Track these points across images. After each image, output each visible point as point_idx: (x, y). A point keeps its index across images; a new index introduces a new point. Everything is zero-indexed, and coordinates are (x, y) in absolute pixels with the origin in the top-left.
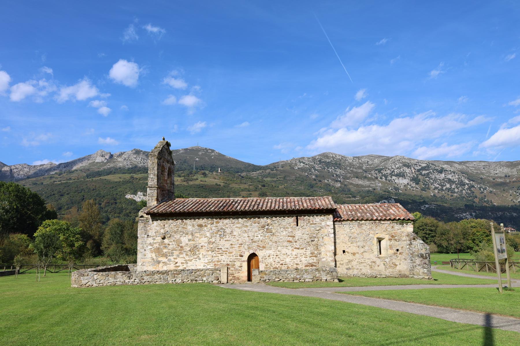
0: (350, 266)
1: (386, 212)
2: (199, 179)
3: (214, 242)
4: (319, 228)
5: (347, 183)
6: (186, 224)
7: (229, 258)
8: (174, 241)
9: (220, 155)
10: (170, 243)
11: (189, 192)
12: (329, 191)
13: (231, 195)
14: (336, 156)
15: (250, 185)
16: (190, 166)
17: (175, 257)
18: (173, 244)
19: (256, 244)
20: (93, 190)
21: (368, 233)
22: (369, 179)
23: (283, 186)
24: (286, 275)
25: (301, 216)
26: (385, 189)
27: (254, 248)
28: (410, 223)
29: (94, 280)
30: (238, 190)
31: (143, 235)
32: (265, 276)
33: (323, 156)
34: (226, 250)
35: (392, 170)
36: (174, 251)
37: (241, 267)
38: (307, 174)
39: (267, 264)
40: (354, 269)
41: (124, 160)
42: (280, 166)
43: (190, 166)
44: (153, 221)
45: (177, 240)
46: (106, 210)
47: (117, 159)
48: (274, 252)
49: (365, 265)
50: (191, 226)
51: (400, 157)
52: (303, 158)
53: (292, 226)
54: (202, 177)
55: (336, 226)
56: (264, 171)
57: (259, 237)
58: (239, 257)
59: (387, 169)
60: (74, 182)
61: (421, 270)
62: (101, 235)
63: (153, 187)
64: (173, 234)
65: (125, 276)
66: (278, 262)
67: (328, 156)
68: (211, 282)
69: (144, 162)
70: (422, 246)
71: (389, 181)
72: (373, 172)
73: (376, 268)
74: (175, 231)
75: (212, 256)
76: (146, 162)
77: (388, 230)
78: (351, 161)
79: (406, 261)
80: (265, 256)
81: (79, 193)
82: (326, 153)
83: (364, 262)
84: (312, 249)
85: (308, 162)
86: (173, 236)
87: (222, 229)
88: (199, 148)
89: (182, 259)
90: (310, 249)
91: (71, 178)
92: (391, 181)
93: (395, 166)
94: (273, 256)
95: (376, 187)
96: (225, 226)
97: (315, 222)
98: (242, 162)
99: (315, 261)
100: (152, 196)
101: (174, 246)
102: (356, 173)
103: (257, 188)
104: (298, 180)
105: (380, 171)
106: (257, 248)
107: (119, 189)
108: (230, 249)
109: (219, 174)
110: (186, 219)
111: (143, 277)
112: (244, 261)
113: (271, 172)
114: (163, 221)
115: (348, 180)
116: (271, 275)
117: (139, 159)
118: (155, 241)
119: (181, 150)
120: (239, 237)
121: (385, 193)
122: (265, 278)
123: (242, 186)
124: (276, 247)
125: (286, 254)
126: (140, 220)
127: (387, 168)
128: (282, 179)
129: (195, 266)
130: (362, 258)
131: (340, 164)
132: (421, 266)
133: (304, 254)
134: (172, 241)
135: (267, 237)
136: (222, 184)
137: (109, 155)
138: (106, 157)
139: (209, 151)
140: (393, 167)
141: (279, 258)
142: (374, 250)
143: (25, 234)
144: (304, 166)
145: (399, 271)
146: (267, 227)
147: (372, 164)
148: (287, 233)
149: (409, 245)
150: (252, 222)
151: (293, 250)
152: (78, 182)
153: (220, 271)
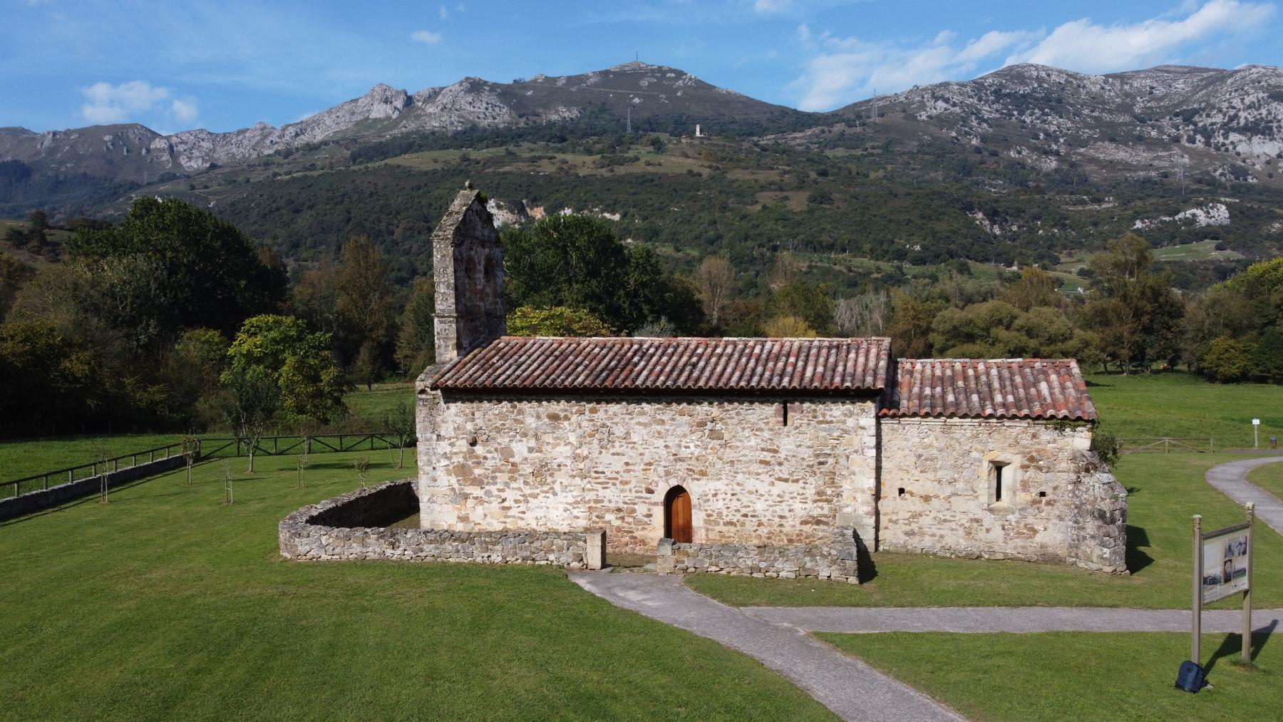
0: (915, 527)
1: (1026, 388)
2: (643, 160)
3: (587, 457)
4: (838, 434)
5: (1079, 158)
6: (521, 412)
7: (622, 495)
8: (496, 450)
9: (700, 85)
10: (489, 456)
11: (614, 197)
12: (1021, 185)
13: (730, 201)
14: (1049, 75)
15: (785, 172)
16: (618, 121)
17: (500, 486)
18: (493, 458)
19: (684, 465)
20: (371, 194)
21: (967, 448)
22: (1151, 144)
23: (881, 173)
24: (735, 559)
25: (792, 402)
26: (1200, 174)
27: (680, 473)
28: (1084, 426)
29: (322, 547)
30: (749, 187)
31: (428, 435)
32: (685, 559)
33: (1007, 75)
34: (615, 475)
35: (1232, 112)
36: (498, 474)
37: (649, 516)
38: (954, 134)
39: (709, 512)
40: (923, 534)
41: (442, 110)
42: (874, 113)
43: (618, 121)
44: (445, 403)
45: (503, 448)
46: (406, 247)
47: (423, 110)
48: (727, 485)
49: (954, 526)
50: (532, 416)
51: (1263, 70)
52: (945, 85)
53: (771, 425)
54: (649, 152)
55: (884, 427)
56: (826, 129)
57: (693, 448)
58: (645, 494)
59: (1215, 112)
60: (323, 174)
61: (1096, 549)
62: (393, 329)
63: (448, 317)
64: (493, 434)
65: (383, 541)
66: (736, 511)
67: (1024, 77)
68: (565, 565)
69: (494, 114)
70: (1104, 490)
71: (1218, 149)
72: (1165, 122)
73: (982, 534)
74: (497, 427)
75: (583, 489)
76: (499, 115)
77: (1023, 442)
78: (1097, 88)
79: (1061, 522)
80: (706, 495)
81: (336, 204)
82: (1018, 66)
83: (952, 519)
84: (821, 483)
85: (961, 98)
86: (494, 439)
87: (604, 426)
88: (641, 69)
89: (516, 492)
90: (814, 482)
91: (314, 165)
92: (1223, 149)
93: (1243, 100)
94: (724, 496)
95: (1173, 167)
96: (612, 419)
97: (828, 418)
98: (763, 103)
99: (826, 512)
100: (446, 338)
101: (498, 461)
102: (1112, 125)
103: (804, 182)
104: (927, 154)
105: (1188, 117)
106: (685, 475)
107: (436, 192)
108: (625, 475)
109: (697, 142)
110: (520, 401)
111: (421, 546)
112: (656, 504)
113: (848, 131)
114: (468, 405)
115: (1082, 150)
116: (700, 557)
117: (480, 107)
118: (455, 450)
119: (591, 74)
120: (644, 446)
121: (1199, 186)
122: (686, 564)
123: (763, 176)
124: (732, 474)
125: (757, 492)
126: (420, 399)
127: (1214, 108)
128: (880, 151)
129: (545, 508)
130: (948, 510)
131: (1059, 101)
132: (1097, 541)
133: (798, 494)
134: (492, 449)
135: (711, 449)
136: (706, 172)
137: (402, 97)
138: (395, 103)
139: (668, 75)
140: (1236, 102)
141: (738, 500)
142: (979, 492)
143: (216, 329)
144: (946, 109)
145: (1042, 547)
146: (710, 425)
147: (1166, 96)
148: (759, 441)
149: (1075, 483)
150: (674, 413)
151: (773, 484)
152: (332, 175)
153: (585, 541)
